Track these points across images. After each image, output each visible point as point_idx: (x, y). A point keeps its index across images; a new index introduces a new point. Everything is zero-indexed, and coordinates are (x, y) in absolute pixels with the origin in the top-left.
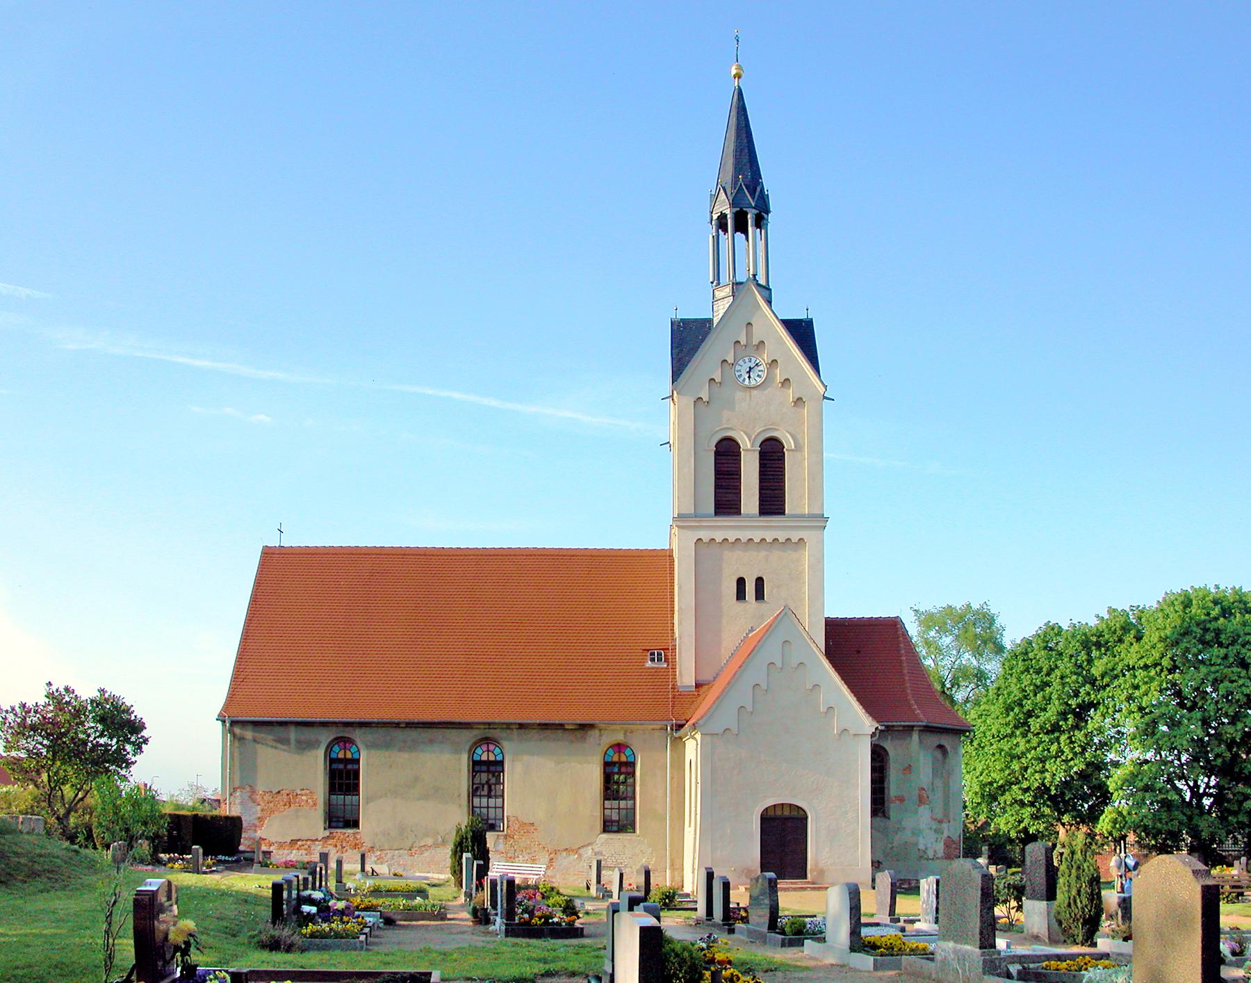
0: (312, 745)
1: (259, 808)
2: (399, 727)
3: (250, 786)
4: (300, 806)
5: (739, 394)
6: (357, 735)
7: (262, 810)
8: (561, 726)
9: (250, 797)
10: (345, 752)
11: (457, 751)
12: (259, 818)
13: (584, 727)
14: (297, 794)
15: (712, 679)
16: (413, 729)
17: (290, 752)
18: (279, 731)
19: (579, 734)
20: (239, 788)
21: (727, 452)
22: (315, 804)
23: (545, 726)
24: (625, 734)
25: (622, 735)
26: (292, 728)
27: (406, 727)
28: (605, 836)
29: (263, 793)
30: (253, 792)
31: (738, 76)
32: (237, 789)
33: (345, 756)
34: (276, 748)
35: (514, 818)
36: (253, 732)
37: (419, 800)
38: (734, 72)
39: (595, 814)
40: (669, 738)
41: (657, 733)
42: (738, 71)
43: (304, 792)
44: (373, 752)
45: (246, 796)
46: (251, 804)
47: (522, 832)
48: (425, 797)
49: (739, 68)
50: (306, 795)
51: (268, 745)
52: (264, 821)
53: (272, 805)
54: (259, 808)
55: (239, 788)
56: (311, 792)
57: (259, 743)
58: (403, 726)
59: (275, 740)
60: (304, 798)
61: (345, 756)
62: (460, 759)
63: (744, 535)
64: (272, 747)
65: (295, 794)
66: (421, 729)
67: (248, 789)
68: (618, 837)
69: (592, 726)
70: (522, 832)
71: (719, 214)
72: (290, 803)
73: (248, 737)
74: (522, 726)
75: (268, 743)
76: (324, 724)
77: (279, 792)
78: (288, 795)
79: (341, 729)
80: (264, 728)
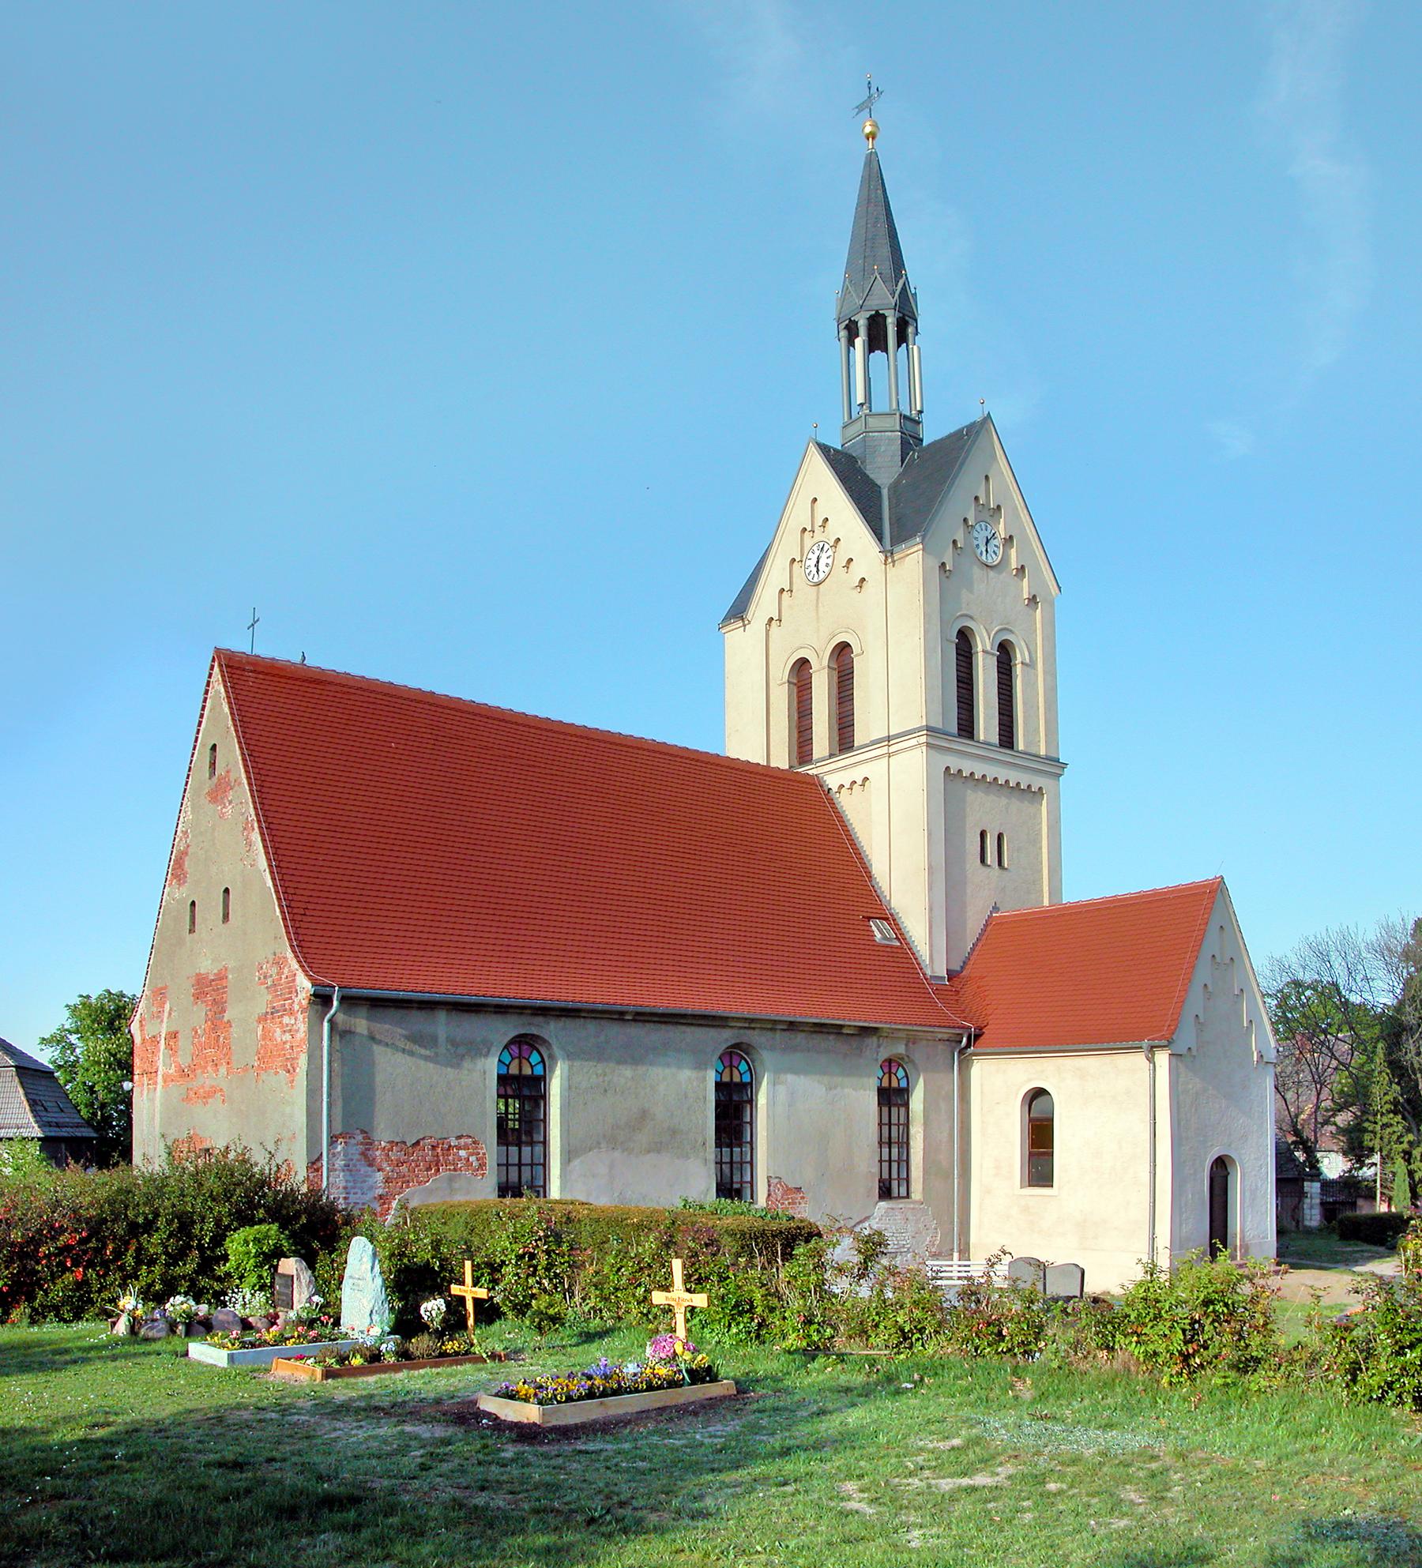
0: (478, 1049)
1: (380, 1176)
2: (623, 1020)
3: (363, 1132)
4: (455, 1170)
5: (977, 572)
6: (550, 1030)
7: (387, 1180)
8: (836, 1030)
9: (362, 1154)
10: (520, 1063)
11: (700, 1066)
12: (381, 1197)
13: (865, 1031)
14: (450, 1146)
15: (959, 969)
16: (640, 1024)
17: (437, 1063)
18: (418, 1021)
19: (855, 1043)
20: (341, 1135)
21: (964, 643)
22: (482, 1166)
23: (820, 1028)
24: (906, 1045)
25: (904, 1046)
26: (442, 1016)
27: (634, 1020)
28: (883, 1204)
29: (389, 1146)
30: (369, 1143)
31: (872, 136)
32: (337, 1137)
33: (520, 1070)
34: (411, 1053)
35: (777, 1180)
36: (368, 1019)
37: (649, 1152)
38: (868, 129)
39: (873, 1171)
40: (956, 1054)
41: (941, 1046)
42: (874, 129)
43: (462, 1141)
44: (577, 1063)
45: (355, 1151)
46: (364, 1169)
47: (786, 1202)
48: (657, 1148)
49: (875, 125)
50: (466, 1147)
51: (394, 1047)
52: (390, 1203)
53: (404, 1169)
54: (380, 1176)
55: (341, 1135)
56: (474, 1143)
57: (379, 1042)
58: (629, 1018)
59: (407, 1038)
60: (462, 1153)
61: (520, 1070)
62: (704, 1078)
63: (979, 769)
64: (404, 1051)
65: (446, 1146)
66: (652, 1026)
67: (360, 1138)
68: (901, 1206)
69: (874, 1031)
70: (786, 1202)
71: (874, 312)
72: (437, 1165)
73: (359, 1030)
74: (792, 1026)
75: (398, 1043)
76: (501, 1010)
77: (418, 1143)
78: (434, 1148)
79: (525, 1019)
80: (392, 1013)
